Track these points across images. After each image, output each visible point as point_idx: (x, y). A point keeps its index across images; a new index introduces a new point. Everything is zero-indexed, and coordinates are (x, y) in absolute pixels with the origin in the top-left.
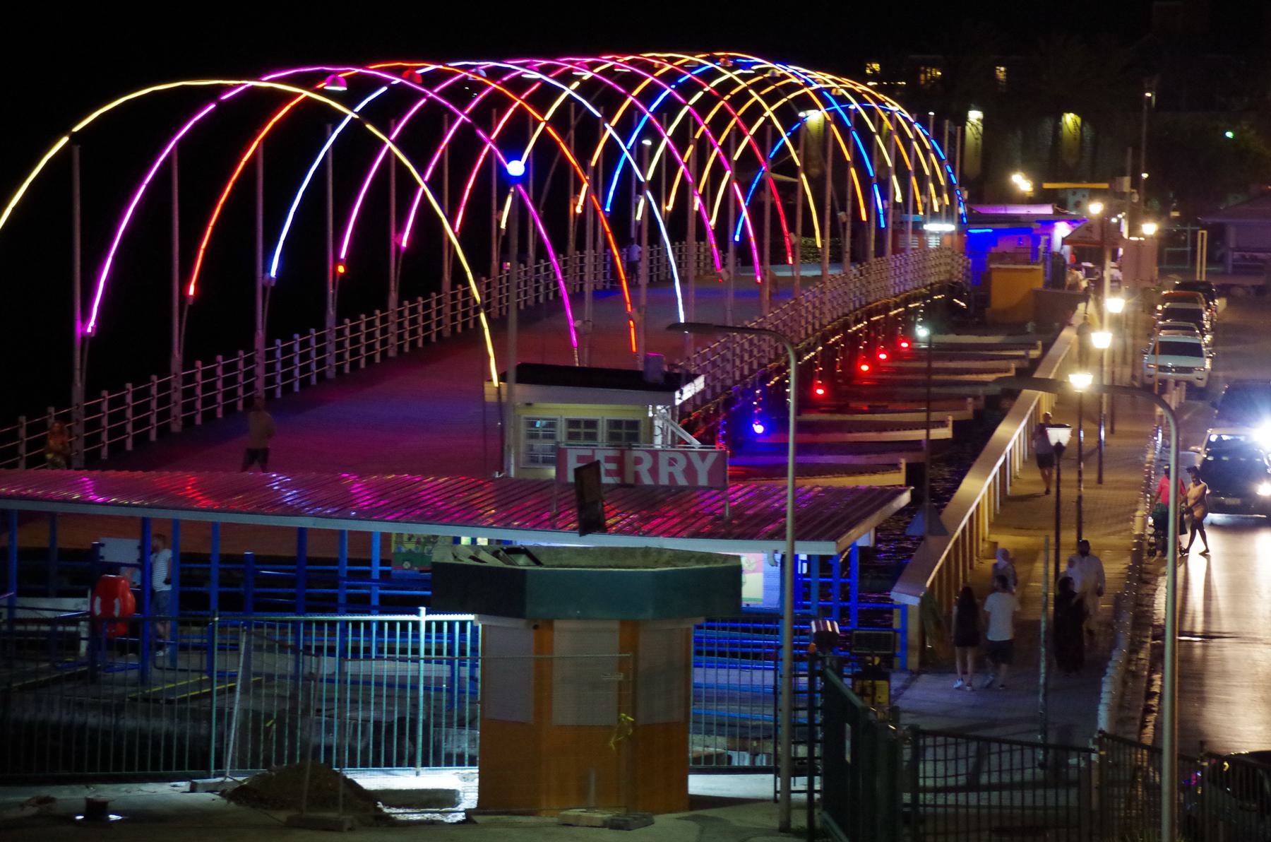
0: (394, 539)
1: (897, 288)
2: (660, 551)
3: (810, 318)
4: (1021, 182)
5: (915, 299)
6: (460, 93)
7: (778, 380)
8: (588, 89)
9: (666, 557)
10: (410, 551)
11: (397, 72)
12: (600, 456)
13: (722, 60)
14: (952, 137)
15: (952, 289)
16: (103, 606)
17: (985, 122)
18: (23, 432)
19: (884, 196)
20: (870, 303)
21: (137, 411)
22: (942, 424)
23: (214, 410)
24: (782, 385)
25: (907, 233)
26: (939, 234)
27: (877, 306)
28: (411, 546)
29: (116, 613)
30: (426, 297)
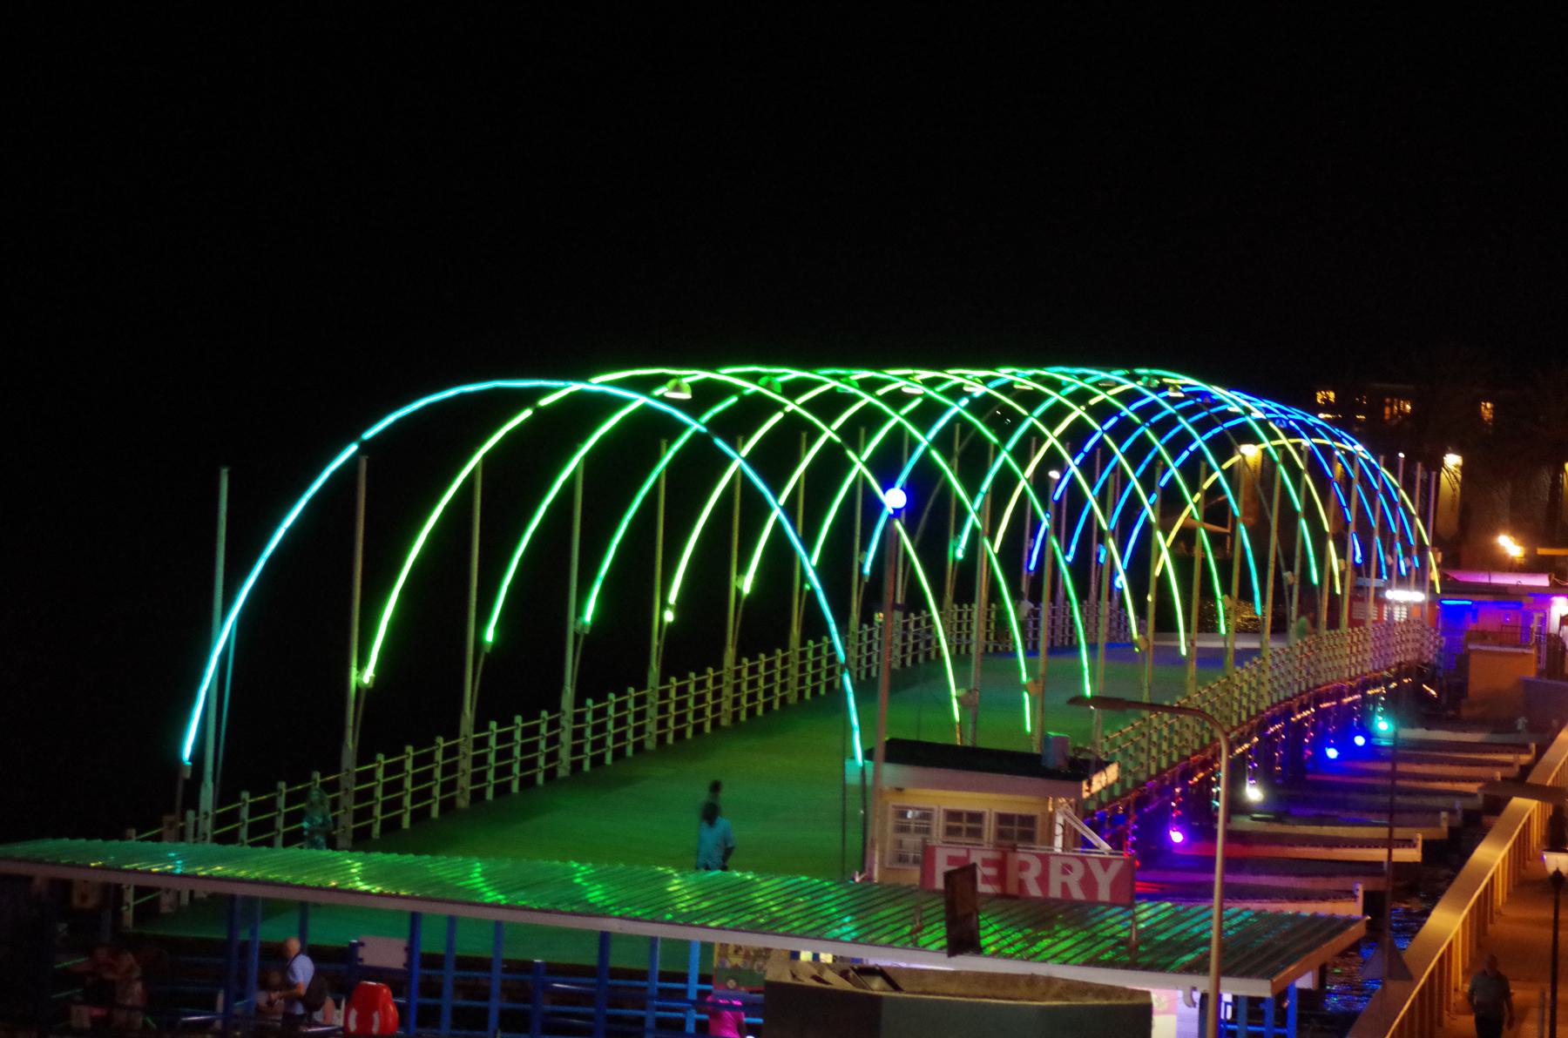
0: (717, 950)
1: (1353, 670)
2: (1049, 981)
3: (1245, 702)
4: (1510, 546)
5: (1376, 684)
6: (829, 405)
7: (1203, 778)
8: (982, 406)
9: (1055, 989)
10: (736, 967)
11: (754, 377)
12: (976, 857)
13: (1145, 379)
14: (1426, 486)
15: (1419, 672)
16: (359, 1020)
17: (1464, 469)
18: (281, 801)
19: (1342, 554)
20: (1319, 687)
21: (417, 780)
22: (1409, 843)
23: (509, 783)
24: (1207, 783)
25: (1368, 600)
26: (1407, 604)
27: (1327, 690)
28: (737, 961)
29: (375, 1030)
30: (770, 653)
